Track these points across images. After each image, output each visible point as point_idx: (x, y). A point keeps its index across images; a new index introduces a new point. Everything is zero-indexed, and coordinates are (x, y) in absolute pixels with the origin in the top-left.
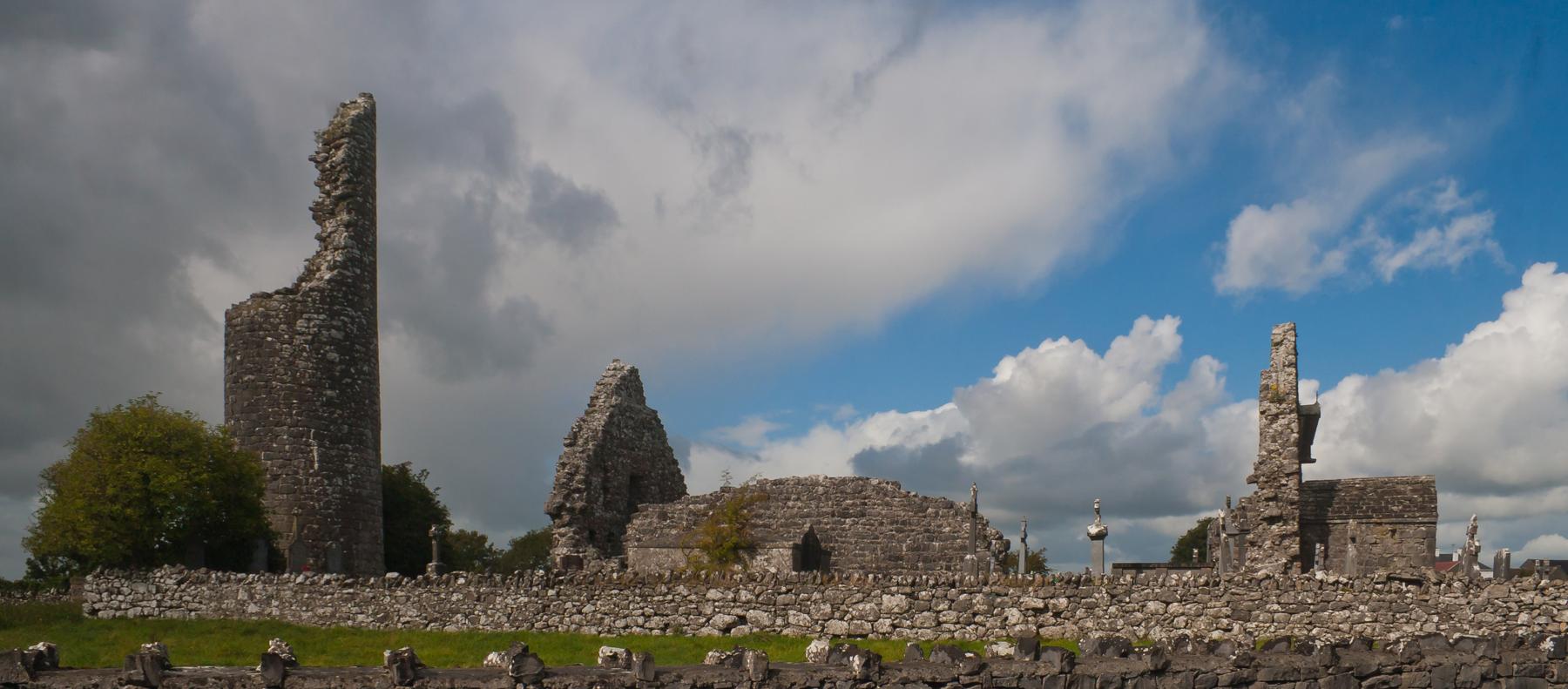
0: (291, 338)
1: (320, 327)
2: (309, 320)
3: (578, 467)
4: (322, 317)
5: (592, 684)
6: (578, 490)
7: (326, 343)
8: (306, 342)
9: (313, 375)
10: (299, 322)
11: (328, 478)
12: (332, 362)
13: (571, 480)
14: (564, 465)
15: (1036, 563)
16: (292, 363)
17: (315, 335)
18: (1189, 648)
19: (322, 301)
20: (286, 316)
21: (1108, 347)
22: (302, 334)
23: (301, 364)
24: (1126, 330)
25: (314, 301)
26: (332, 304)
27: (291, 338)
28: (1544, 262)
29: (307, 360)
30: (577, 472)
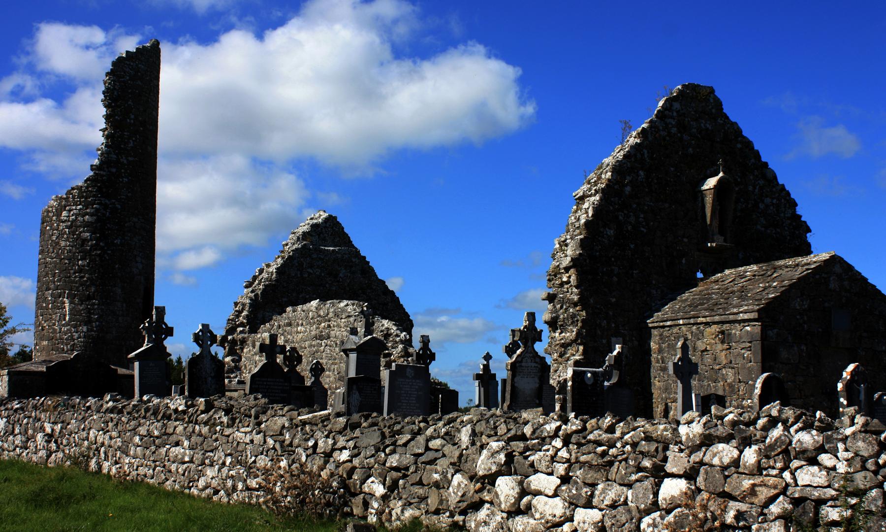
0: (58, 225)
1: (76, 215)
2: (70, 211)
3: (244, 305)
4: (79, 207)
5: (180, 530)
6: (242, 325)
7: (80, 226)
8: (67, 227)
9: (70, 251)
10: (64, 213)
11: (75, 326)
12: (84, 241)
13: (238, 316)
14: (236, 304)
15: (70, 497)
16: (58, 243)
17: (73, 221)
18: (739, 146)
19: (80, 197)
20: (57, 210)
21: (809, 245)
22: (63, 222)
23: (63, 244)
24: (107, 117)
25: (74, 197)
26: (86, 198)
27: (58, 225)
28: (508, 62)
29: (67, 240)
30: (243, 309)
